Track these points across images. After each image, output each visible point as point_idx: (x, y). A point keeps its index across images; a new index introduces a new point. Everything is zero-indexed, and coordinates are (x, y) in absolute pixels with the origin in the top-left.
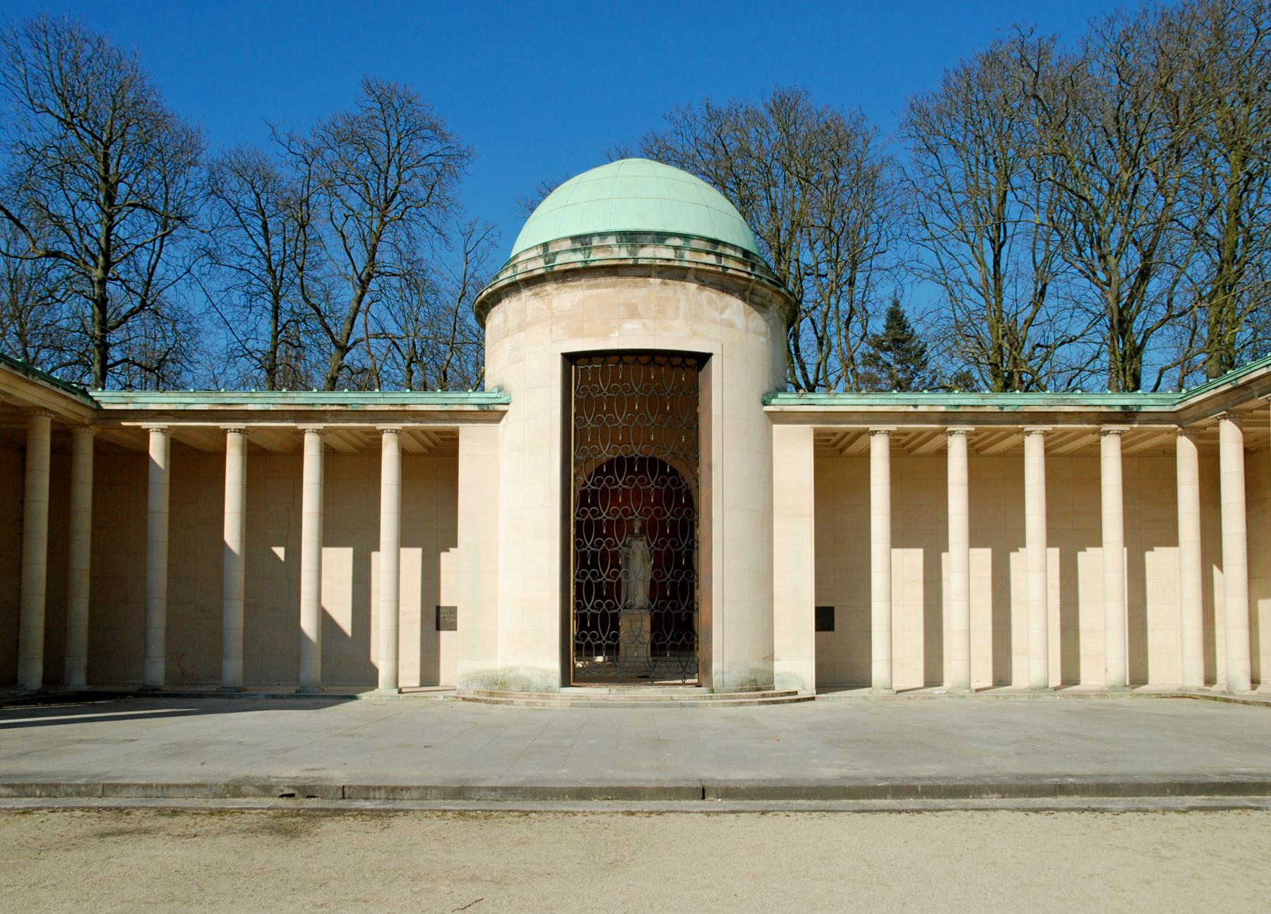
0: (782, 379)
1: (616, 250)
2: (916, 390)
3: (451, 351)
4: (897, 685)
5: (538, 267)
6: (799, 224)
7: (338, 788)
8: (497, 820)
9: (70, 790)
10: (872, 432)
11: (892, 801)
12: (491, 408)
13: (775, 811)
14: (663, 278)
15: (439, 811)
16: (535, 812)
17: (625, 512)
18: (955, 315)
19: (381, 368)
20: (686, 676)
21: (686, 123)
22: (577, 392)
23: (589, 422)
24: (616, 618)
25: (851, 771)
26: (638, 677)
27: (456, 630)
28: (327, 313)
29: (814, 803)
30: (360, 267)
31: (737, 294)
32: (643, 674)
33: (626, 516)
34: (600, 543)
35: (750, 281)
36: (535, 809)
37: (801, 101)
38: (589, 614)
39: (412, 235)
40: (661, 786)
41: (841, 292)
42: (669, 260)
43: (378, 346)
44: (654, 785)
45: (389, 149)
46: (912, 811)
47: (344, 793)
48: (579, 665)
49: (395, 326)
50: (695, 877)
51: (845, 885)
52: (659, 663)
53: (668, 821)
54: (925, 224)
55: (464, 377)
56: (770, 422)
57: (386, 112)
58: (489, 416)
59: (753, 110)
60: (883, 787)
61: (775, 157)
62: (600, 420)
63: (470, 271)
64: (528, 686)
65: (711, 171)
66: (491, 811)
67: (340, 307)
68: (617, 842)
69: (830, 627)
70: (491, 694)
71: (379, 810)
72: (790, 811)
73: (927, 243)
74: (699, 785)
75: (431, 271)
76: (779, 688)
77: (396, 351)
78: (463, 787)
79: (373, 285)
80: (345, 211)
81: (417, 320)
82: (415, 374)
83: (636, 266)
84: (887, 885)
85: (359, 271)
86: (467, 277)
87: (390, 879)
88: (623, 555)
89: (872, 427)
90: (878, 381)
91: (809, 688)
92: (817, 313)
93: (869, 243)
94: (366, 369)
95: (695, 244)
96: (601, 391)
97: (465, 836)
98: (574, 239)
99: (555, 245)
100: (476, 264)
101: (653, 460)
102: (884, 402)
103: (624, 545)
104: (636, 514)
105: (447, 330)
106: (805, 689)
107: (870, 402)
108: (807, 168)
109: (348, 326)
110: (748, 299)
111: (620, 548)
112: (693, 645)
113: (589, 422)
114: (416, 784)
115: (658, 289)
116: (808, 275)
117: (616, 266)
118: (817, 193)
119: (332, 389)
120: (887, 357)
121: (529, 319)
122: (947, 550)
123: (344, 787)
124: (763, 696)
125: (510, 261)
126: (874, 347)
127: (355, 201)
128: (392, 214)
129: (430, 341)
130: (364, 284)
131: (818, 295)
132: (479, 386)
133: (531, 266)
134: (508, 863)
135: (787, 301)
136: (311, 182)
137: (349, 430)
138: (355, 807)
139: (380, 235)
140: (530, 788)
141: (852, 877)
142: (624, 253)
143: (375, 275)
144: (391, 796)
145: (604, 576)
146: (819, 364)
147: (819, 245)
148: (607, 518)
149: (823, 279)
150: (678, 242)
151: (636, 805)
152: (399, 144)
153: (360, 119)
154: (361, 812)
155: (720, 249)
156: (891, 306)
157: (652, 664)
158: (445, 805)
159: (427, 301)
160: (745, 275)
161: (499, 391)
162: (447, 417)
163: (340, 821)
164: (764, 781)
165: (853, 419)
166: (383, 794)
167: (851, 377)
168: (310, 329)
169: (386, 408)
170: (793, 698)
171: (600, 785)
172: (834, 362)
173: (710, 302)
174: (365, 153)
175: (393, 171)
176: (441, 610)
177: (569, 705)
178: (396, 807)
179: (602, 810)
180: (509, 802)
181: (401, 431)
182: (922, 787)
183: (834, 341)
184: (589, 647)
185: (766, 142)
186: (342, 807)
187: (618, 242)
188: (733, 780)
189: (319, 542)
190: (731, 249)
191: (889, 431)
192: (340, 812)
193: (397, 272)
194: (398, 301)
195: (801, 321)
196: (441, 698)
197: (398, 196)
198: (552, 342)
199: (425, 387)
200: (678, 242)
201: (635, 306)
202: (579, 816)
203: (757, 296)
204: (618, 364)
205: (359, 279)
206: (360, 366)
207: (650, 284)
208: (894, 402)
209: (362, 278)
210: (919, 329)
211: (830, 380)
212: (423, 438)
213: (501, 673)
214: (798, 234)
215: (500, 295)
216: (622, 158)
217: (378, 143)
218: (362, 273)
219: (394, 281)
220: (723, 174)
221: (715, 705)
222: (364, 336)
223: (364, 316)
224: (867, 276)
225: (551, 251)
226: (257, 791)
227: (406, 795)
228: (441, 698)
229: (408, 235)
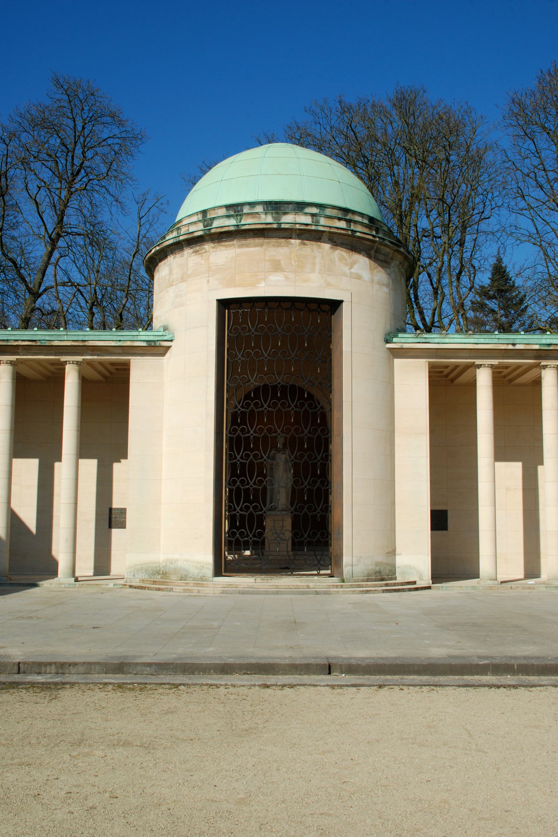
0: (403, 322)
1: (263, 216)
2: (517, 331)
3: (126, 297)
4: (501, 577)
5: (198, 229)
7: (14, 664)
8: (151, 692)
10: (478, 365)
11: (492, 677)
12: (158, 344)
13: (391, 685)
14: (302, 239)
15: (101, 683)
16: (184, 685)
17: (270, 430)
18: (548, 270)
19: (67, 311)
22: (229, 331)
23: (240, 356)
24: (261, 519)
25: (458, 651)
26: (281, 568)
27: (125, 527)
28: (23, 265)
29: (425, 678)
31: (363, 253)
32: (284, 566)
34: (248, 456)
35: (374, 242)
36: (184, 682)
37: (418, 98)
38: (238, 515)
39: (94, 202)
40: (293, 662)
42: (307, 225)
43: (66, 292)
44: (287, 662)
45: (75, 133)
46: (509, 686)
47: (19, 668)
48: (230, 557)
50: (318, 743)
51: (448, 751)
53: (298, 693)
54: (523, 197)
55: (137, 318)
56: (391, 356)
57: (73, 103)
58: (155, 350)
59: (379, 104)
60: (484, 665)
61: (398, 141)
62: (249, 354)
63: (143, 232)
64: (186, 576)
66: (146, 684)
67: (33, 260)
70: (154, 582)
71: (49, 683)
72: (403, 685)
73: (524, 212)
74: (325, 662)
75: (110, 232)
77: (80, 296)
79: (61, 243)
80: (38, 182)
81: (98, 272)
82: (96, 316)
83: (279, 229)
84: (484, 752)
86: (141, 237)
87: (53, 745)
89: (478, 362)
90: (484, 324)
91: (425, 578)
92: (433, 268)
93: (476, 212)
94: (55, 311)
95: (328, 212)
96: (250, 331)
97: (122, 706)
98: (228, 207)
99: (213, 212)
100: (148, 226)
101: (293, 386)
103: (268, 457)
104: (279, 431)
105: (124, 281)
106: (422, 580)
107: (476, 341)
108: (424, 151)
109: (39, 276)
110: (373, 256)
111: (265, 460)
112: (327, 542)
113: (240, 356)
114: (82, 660)
116: (426, 237)
119: (26, 328)
120: (493, 304)
121: (190, 272)
122: (542, 464)
123: (19, 663)
124: (387, 585)
126: (480, 297)
127: (46, 175)
128: (77, 186)
130: (53, 242)
131: (434, 253)
132: (148, 325)
133: (192, 229)
134: (157, 730)
135: (406, 258)
136: (9, 160)
137: (38, 362)
138: (27, 680)
139: (68, 202)
140: (181, 664)
141: (454, 744)
142: (269, 219)
144: (60, 671)
145: (251, 483)
147: (434, 213)
148: (254, 435)
149: (438, 240)
150: (314, 210)
151: (271, 679)
152: (83, 128)
153: (50, 108)
154: (33, 685)
155: (350, 216)
156: (495, 262)
157: (292, 558)
158: (107, 678)
160: (371, 237)
161: (164, 330)
162: (120, 351)
163: (14, 693)
164: (382, 659)
165: (462, 355)
167: (461, 320)
168: (8, 277)
169: (69, 344)
172: (447, 308)
173: (342, 259)
174: (55, 136)
175: (78, 151)
176: (113, 511)
177: (220, 592)
178: (64, 681)
179: (242, 683)
180: (162, 676)
181: (81, 362)
182: (518, 665)
183: (447, 291)
184: (238, 542)
185: (390, 130)
186: (17, 680)
187: (264, 210)
188: (355, 658)
189: (10, 454)
190: (359, 216)
191: (492, 365)
192: (15, 685)
193: (82, 232)
194: (82, 256)
195: (419, 274)
196: (111, 585)
198: (210, 290)
199: (104, 326)
200: (314, 210)
201: (279, 261)
203: (381, 254)
204: (264, 308)
205: (50, 237)
206: (50, 308)
207: (291, 244)
208: (496, 341)
209: (52, 237)
210: (519, 282)
211: (444, 323)
213: (163, 564)
214: (417, 204)
215: (166, 252)
216: (270, 142)
217: (66, 127)
218: (52, 233)
219: (80, 240)
220: (354, 155)
221: (345, 593)
222: (53, 284)
225: (208, 217)
228: (111, 585)
229: (91, 203)
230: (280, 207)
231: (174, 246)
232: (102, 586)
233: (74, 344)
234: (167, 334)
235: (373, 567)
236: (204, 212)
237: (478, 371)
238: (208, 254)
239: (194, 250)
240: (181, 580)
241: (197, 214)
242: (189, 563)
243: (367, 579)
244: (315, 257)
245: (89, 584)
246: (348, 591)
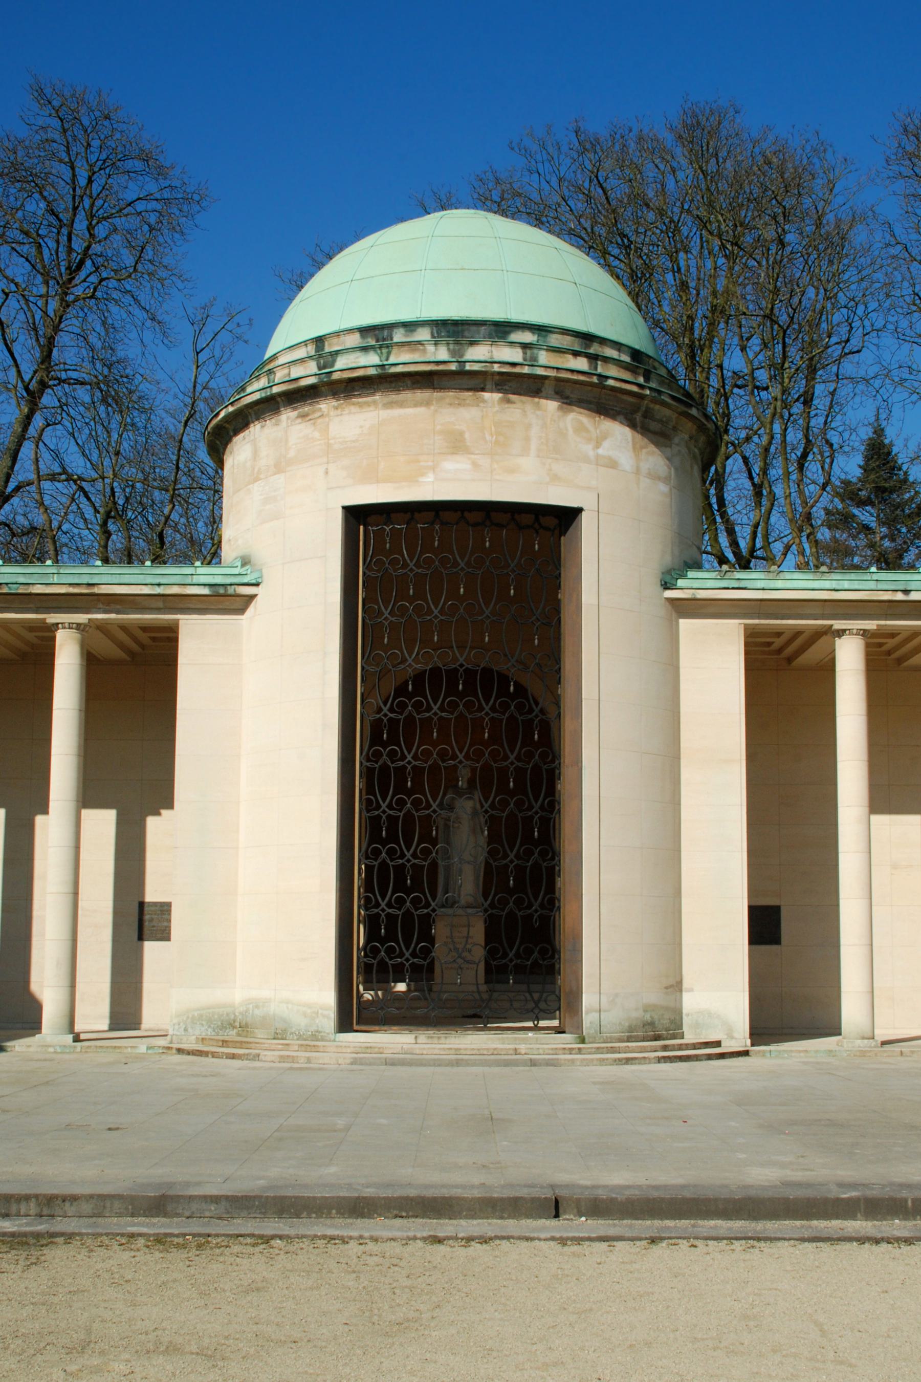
0: (695, 549)
1: (431, 348)
4: (882, 1033)
5: (308, 374)
6: (722, 312)
8: (218, 1251)
11: (864, 1223)
12: (231, 590)
13: (674, 1238)
14: (505, 392)
15: (122, 1235)
16: (281, 1237)
17: (443, 755)
19: (60, 527)
20: (541, 1014)
21: (545, 157)
22: (367, 567)
23: (386, 614)
24: (427, 922)
25: (800, 1174)
26: (464, 1017)
27: (168, 939)
29: (738, 1225)
30: (27, 370)
31: (621, 417)
32: (470, 1012)
33: (444, 761)
34: (401, 802)
36: (280, 1233)
37: (725, 123)
39: (110, 321)
40: (488, 1195)
41: (790, 415)
42: (514, 365)
44: (477, 1193)
45: (74, 190)
46: (898, 1240)
48: (368, 996)
49: (81, 461)
50: (535, 1347)
52: (495, 995)
53: (497, 1253)
55: (192, 541)
56: (674, 615)
57: (69, 133)
58: (227, 603)
60: (849, 1199)
61: (686, 207)
63: (203, 378)
64: (285, 1031)
65: (585, 229)
66: (209, 1236)
68: (411, 1289)
69: (775, 939)
70: (225, 1043)
71: (25, 1235)
72: (696, 1238)
74: (549, 1194)
75: (140, 378)
77: (83, 500)
78: (164, 1197)
79: (48, 399)
81: (117, 453)
82: (114, 537)
84: (851, 1365)
85: (27, 378)
86: (199, 388)
88: (441, 823)
89: (838, 625)
94: (36, 528)
95: (555, 340)
96: (405, 565)
97: (163, 1278)
98: (365, 331)
99: (335, 340)
100: (212, 367)
101: (488, 672)
102: (856, 585)
103: (441, 806)
104: (461, 757)
107: (834, 585)
110: (639, 424)
111: (434, 811)
112: (553, 965)
113: (386, 614)
114: (87, 1191)
115: (496, 408)
116: (739, 387)
117: (430, 374)
118: (752, 263)
120: (866, 516)
121: (292, 454)
124: (665, 1048)
125: (265, 364)
126: (842, 501)
128: (79, 291)
129: (138, 485)
130: (33, 398)
131: (755, 419)
132: (213, 556)
133: (296, 372)
134: (230, 1323)
135: (702, 428)
139: (60, 322)
140: (275, 1197)
141: (793, 1350)
142: (442, 354)
143: (51, 383)
146: (756, 526)
147: (756, 342)
148: (414, 763)
149: (763, 394)
150: (528, 337)
151: (446, 1227)
152: (90, 181)
153: (27, 143)
155: (595, 349)
156: (871, 435)
157: (485, 996)
158: (134, 1225)
159: (133, 425)
160: (635, 389)
161: (243, 565)
162: (160, 604)
164: (656, 1188)
166: (33, 1208)
167: (806, 546)
171: (389, 1193)
173: (580, 429)
174: (36, 196)
175: (81, 225)
176: (146, 909)
177: (349, 1061)
178: (52, 1230)
180: (239, 1221)
181: (85, 625)
182: (914, 1201)
183: (778, 490)
185: (671, 184)
187: (433, 336)
188: (605, 1187)
190: (612, 348)
191: (864, 630)
193: (87, 378)
194: (87, 424)
195: (727, 458)
196: (143, 1049)
197: (88, 263)
198: (329, 489)
199: (129, 557)
200: (528, 337)
201: (461, 434)
202: (353, 1243)
203: (654, 420)
204: (432, 523)
205: (27, 389)
206: (26, 523)
207: (484, 401)
208: (872, 585)
209: (31, 387)
211: (775, 551)
212: (122, 636)
215: (247, 417)
216: (443, 208)
217: (56, 180)
218: (31, 380)
219: (83, 394)
220: (603, 232)
222: (33, 476)
223: (33, 446)
224: (831, 389)
225: (327, 349)
227: (70, 1209)
228: (143, 1049)
229: (104, 323)
230: (463, 331)
231: (261, 406)
232: (125, 1051)
234: (249, 572)
236: (319, 341)
238: (327, 419)
240: (274, 1039)
241: (306, 345)
244: (529, 427)
245: (101, 1047)
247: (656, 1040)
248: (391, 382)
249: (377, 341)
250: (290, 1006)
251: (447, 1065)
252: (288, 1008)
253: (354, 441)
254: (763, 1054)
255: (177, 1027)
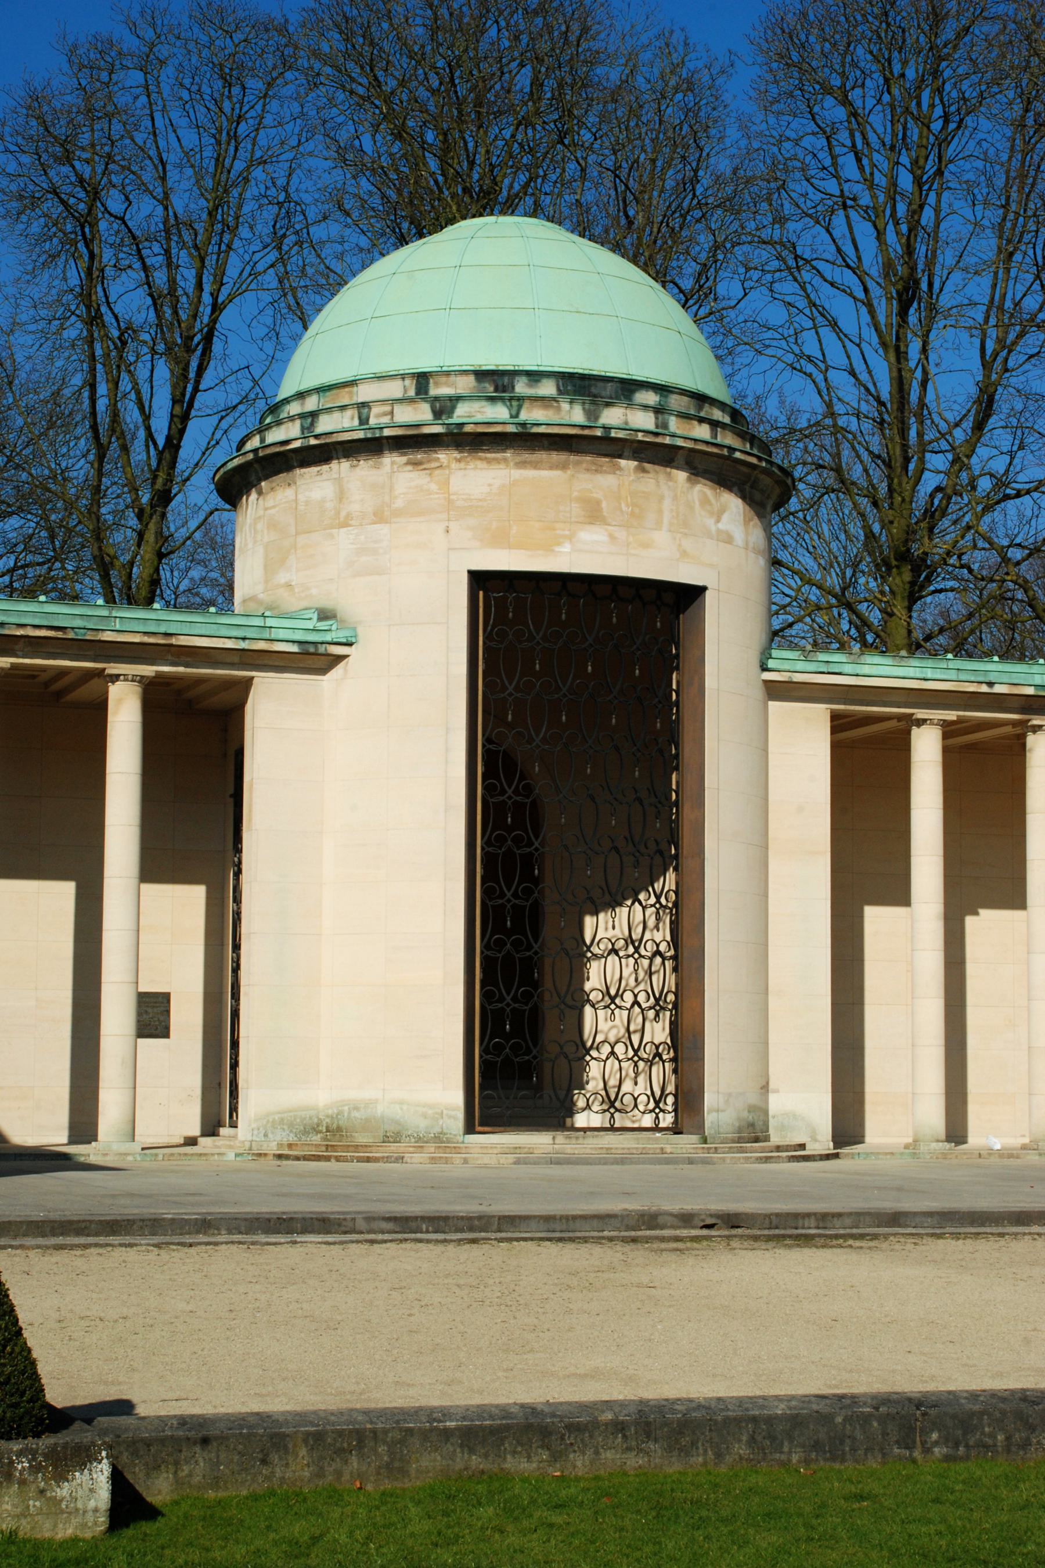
9: (461, 1224)
12: (322, 649)
14: (640, 460)
31: (735, 489)
58: (310, 662)
76: (775, 1139)
89: (920, 714)
98: (481, 375)
121: (399, 503)
150: (651, 398)
160: (754, 461)
166: (813, 1222)
169: (137, 639)
170: (798, 1153)
173: (705, 502)
177: (511, 1161)
190: (719, 408)
201: (598, 503)
207: (620, 469)
208: (952, 675)
226: (675, 1221)
227: (837, 1222)
230: (590, 386)
232: (212, 1158)
233: (146, 639)
234: (334, 627)
235: (745, 1114)
237: (915, 731)
238: (447, 472)
239: (409, 459)
241: (403, 379)
242: (405, 1107)
243: (739, 1138)
244: (661, 498)
245: (186, 1154)
246: (739, 1158)
247: (756, 1142)
248: (526, 440)
249: (496, 390)
250: (405, 1107)
251: (612, 1164)
252: (402, 1109)
253: (480, 500)
254: (852, 1156)
255: (255, 1132)
